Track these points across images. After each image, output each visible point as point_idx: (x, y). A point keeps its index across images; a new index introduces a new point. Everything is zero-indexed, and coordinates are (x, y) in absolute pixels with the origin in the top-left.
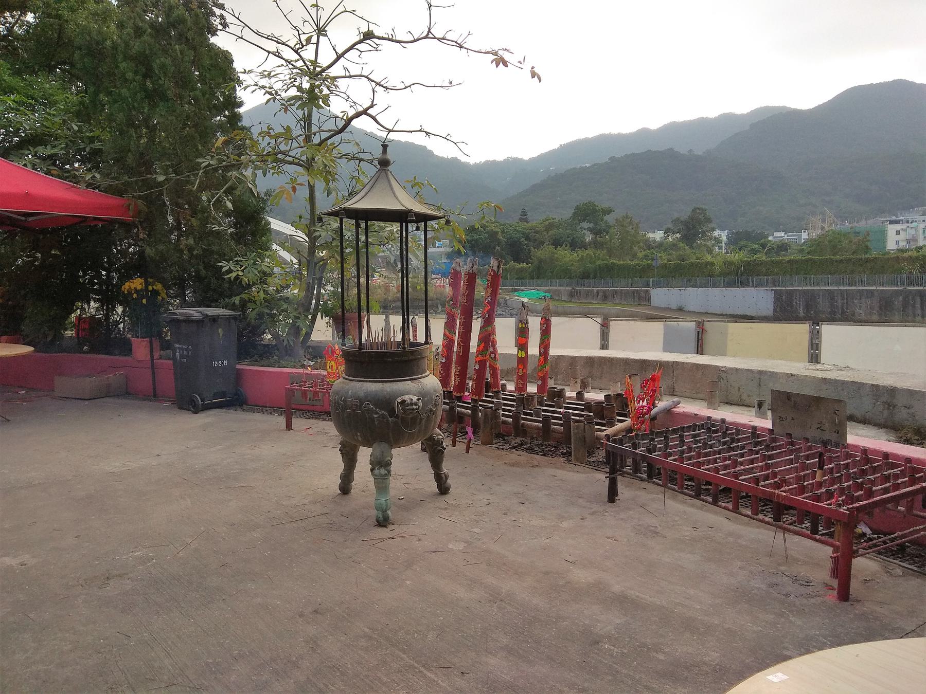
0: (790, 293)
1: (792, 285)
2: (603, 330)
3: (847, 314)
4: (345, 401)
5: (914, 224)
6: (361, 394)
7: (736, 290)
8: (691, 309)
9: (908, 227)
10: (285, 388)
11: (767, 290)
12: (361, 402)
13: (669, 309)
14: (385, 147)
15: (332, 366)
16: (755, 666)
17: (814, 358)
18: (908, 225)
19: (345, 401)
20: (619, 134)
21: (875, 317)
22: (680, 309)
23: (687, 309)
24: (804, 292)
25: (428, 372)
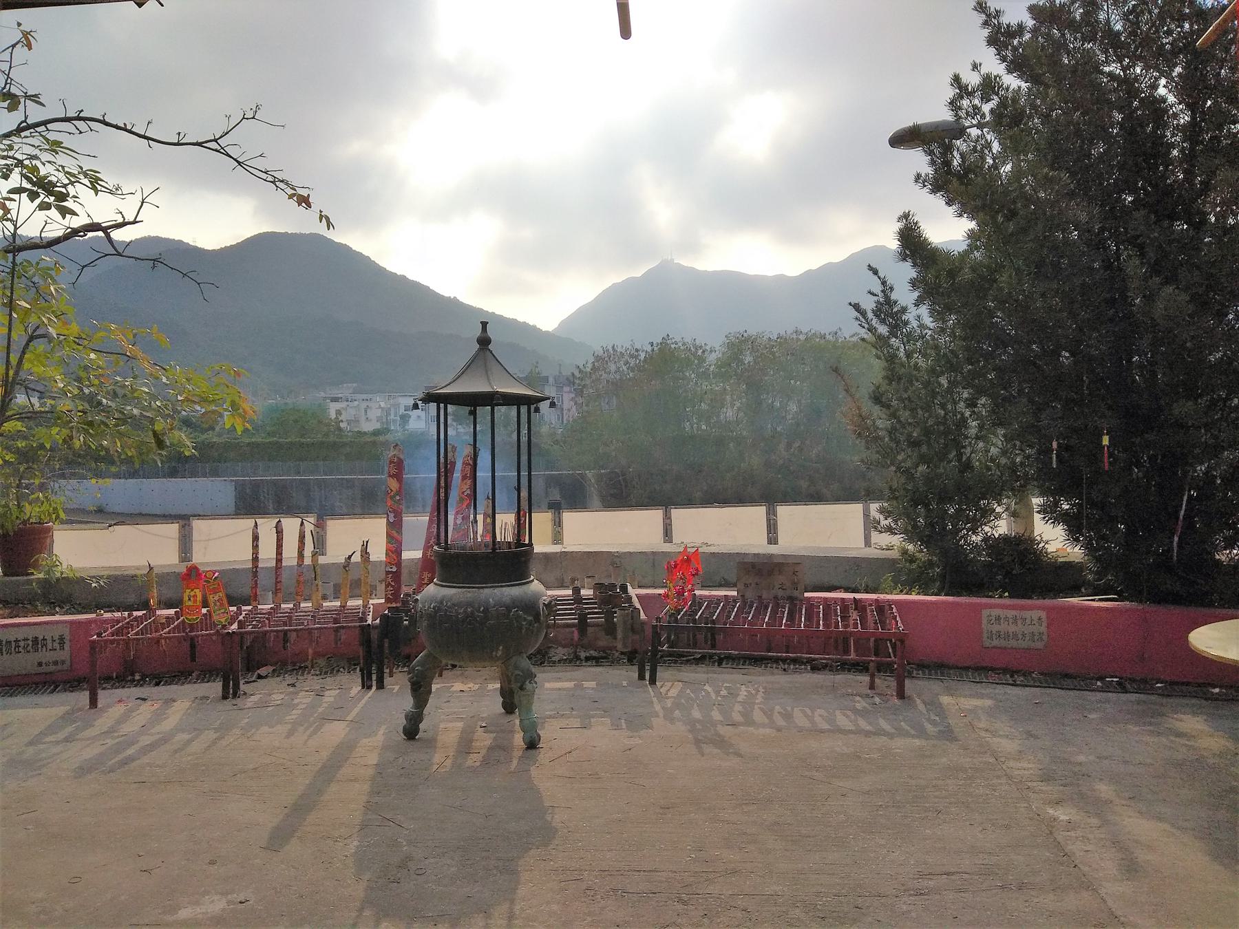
0: (256, 486)
1: (255, 474)
2: (318, 532)
3: (326, 508)
4: (486, 611)
5: (356, 403)
6: (507, 600)
7: (205, 480)
8: (117, 509)
9: (348, 406)
10: (90, 641)
11: (225, 480)
12: (508, 609)
13: (83, 511)
14: (484, 324)
15: (195, 596)
16: (160, 914)
17: (773, 540)
18: (347, 403)
19: (486, 611)
20: (534, 327)
21: (358, 510)
22: (100, 511)
23: (110, 509)
24: (274, 483)
25: (532, 577)
